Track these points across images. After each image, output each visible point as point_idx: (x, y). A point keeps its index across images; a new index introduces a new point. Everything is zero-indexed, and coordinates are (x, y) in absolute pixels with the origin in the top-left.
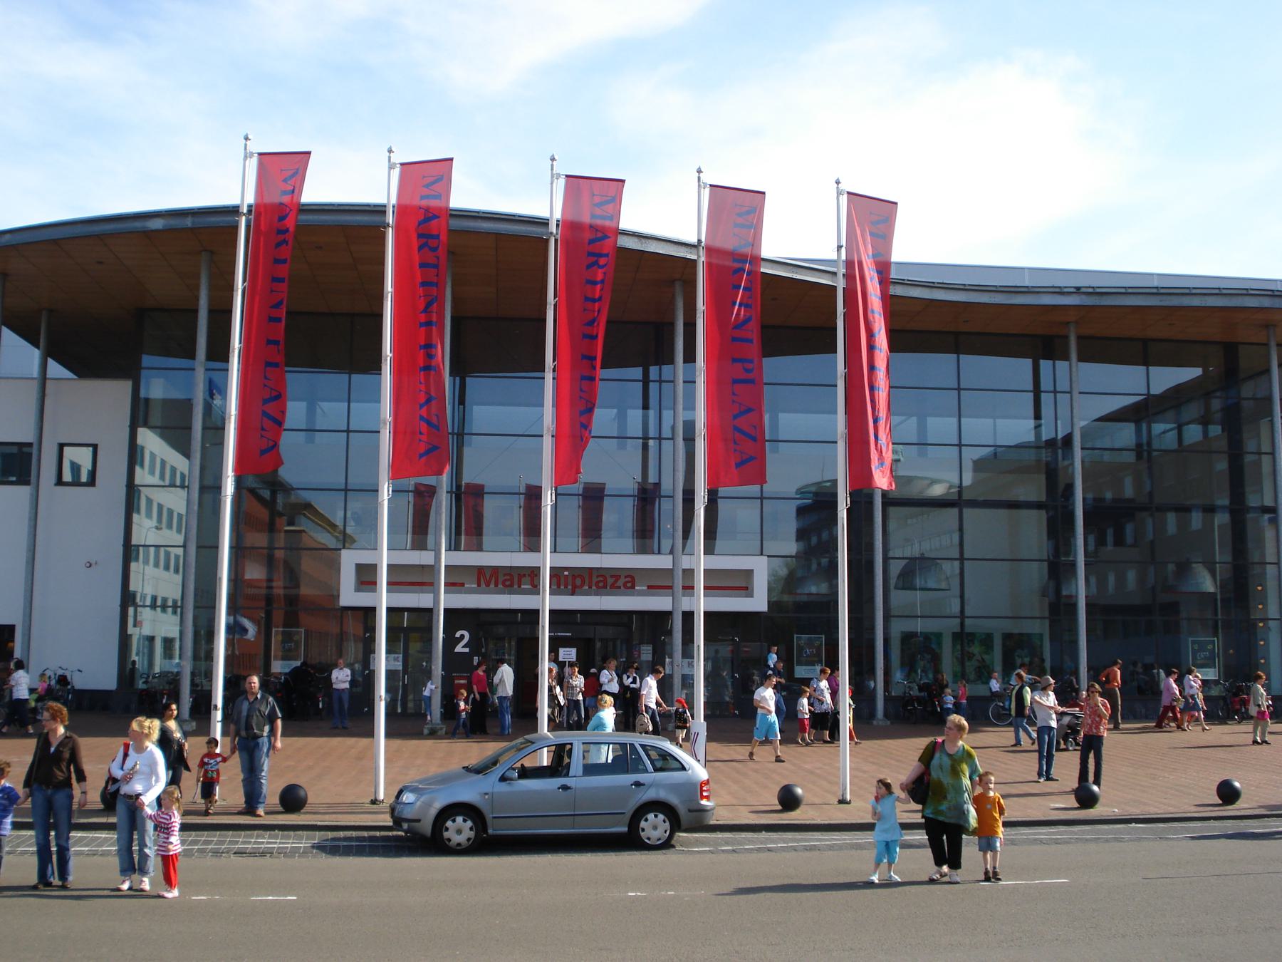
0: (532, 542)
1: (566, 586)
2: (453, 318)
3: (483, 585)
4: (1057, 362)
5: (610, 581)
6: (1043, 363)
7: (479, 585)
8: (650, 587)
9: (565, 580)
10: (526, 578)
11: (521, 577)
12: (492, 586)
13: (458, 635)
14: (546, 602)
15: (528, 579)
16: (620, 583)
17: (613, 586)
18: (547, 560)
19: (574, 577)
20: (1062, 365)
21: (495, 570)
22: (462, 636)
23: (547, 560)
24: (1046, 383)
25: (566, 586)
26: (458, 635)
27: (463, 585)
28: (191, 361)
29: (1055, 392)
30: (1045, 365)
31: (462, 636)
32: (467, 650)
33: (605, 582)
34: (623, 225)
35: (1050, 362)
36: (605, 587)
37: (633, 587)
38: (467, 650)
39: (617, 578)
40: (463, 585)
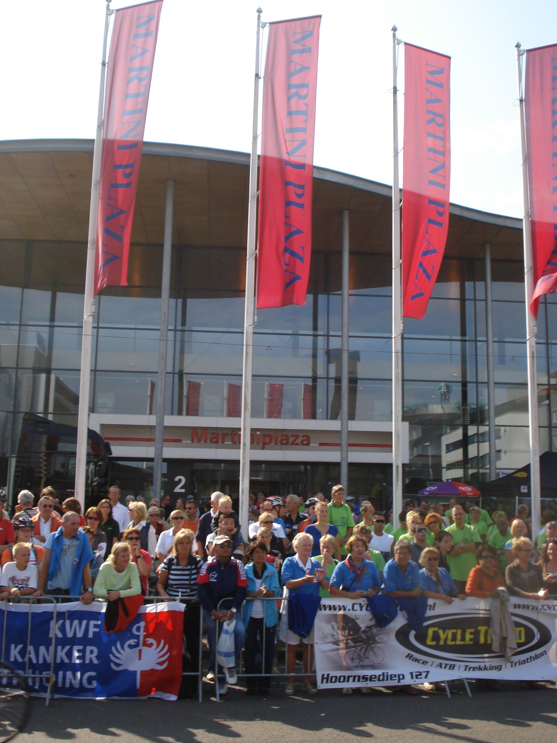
0: (234, 411)
1: (258, 443)
2: (173, 246)
3: (196, 440)
4: (477, 283)
5: (291, 440)
6: (467, 283)
7: (193, 441)
8: (321, 444)
9: (261, 438)
10: (231, 436)
11: (224, 435)
12: (202, 442)
13: (177, 479)
14: (245, 454)
15: (229, 437)
16: (298, 441)
17: (293, 443)
18: (245, 423)
19: (265, 436)
20: (480, 285)
21: (205, 429)
22: (180, 481)
23: (245, 423)
24: (469, 294)
25: (258, 443)
26: (177, 479)
27: (180, 441)
28: (72, 445)
29: (475, 300)
30: (469, 285)
31: (180, 481)
32: (183, 491)
33: (287, 439)
34: (316, 164)
35: (472, 283)
36: (287, 444)
37: (308, 444)
38: (183, 491)
39: (297, 437)
40: (180, 441)
